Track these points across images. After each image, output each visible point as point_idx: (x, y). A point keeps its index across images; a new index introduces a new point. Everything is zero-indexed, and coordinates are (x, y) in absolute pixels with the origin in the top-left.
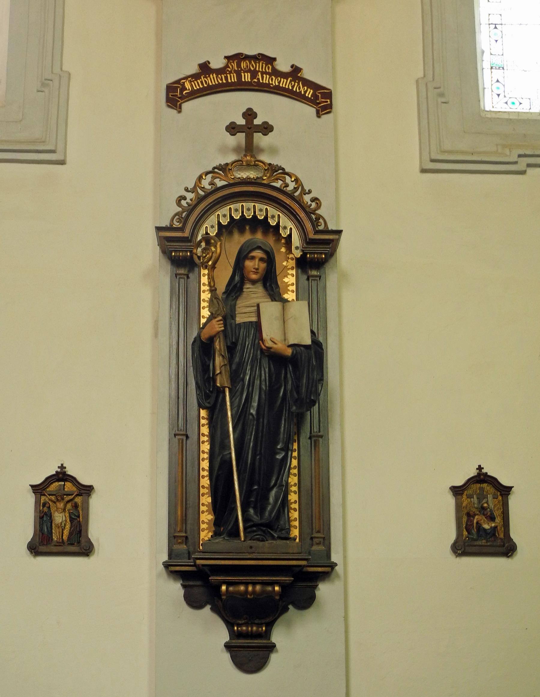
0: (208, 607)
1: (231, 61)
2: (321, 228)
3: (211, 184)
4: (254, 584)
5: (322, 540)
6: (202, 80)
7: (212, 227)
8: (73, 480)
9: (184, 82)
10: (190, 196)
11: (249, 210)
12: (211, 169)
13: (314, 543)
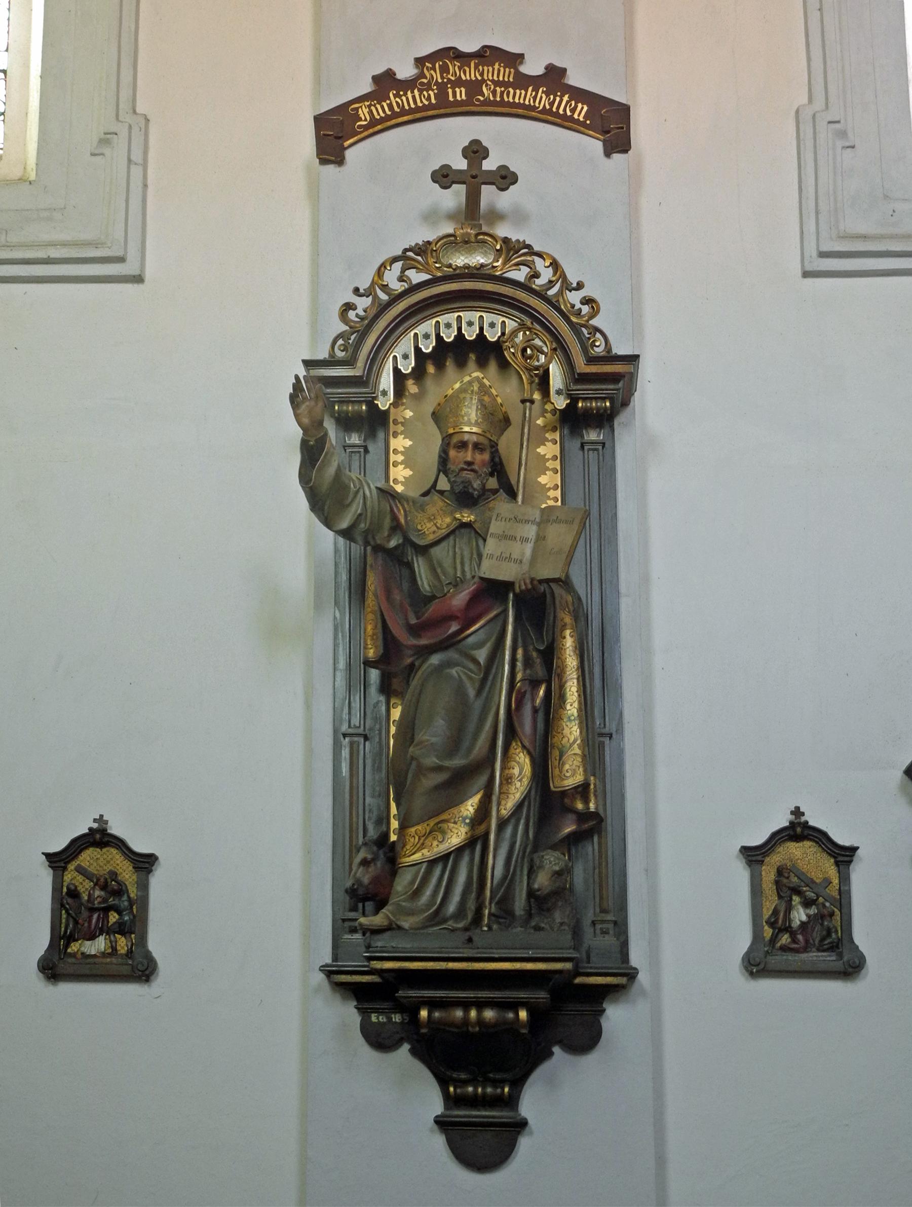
0: (406, 1047)
2: (600, 350)
3: (401, 279)
4: (481, 1005)
5: (611, 926)
6: (391, 103)
7: (406, 357)
8: (120, 844)
9: (357, 109)
10: (363, 303)
11: (448, 326)
12: (400, 253)
13: (598, 931)
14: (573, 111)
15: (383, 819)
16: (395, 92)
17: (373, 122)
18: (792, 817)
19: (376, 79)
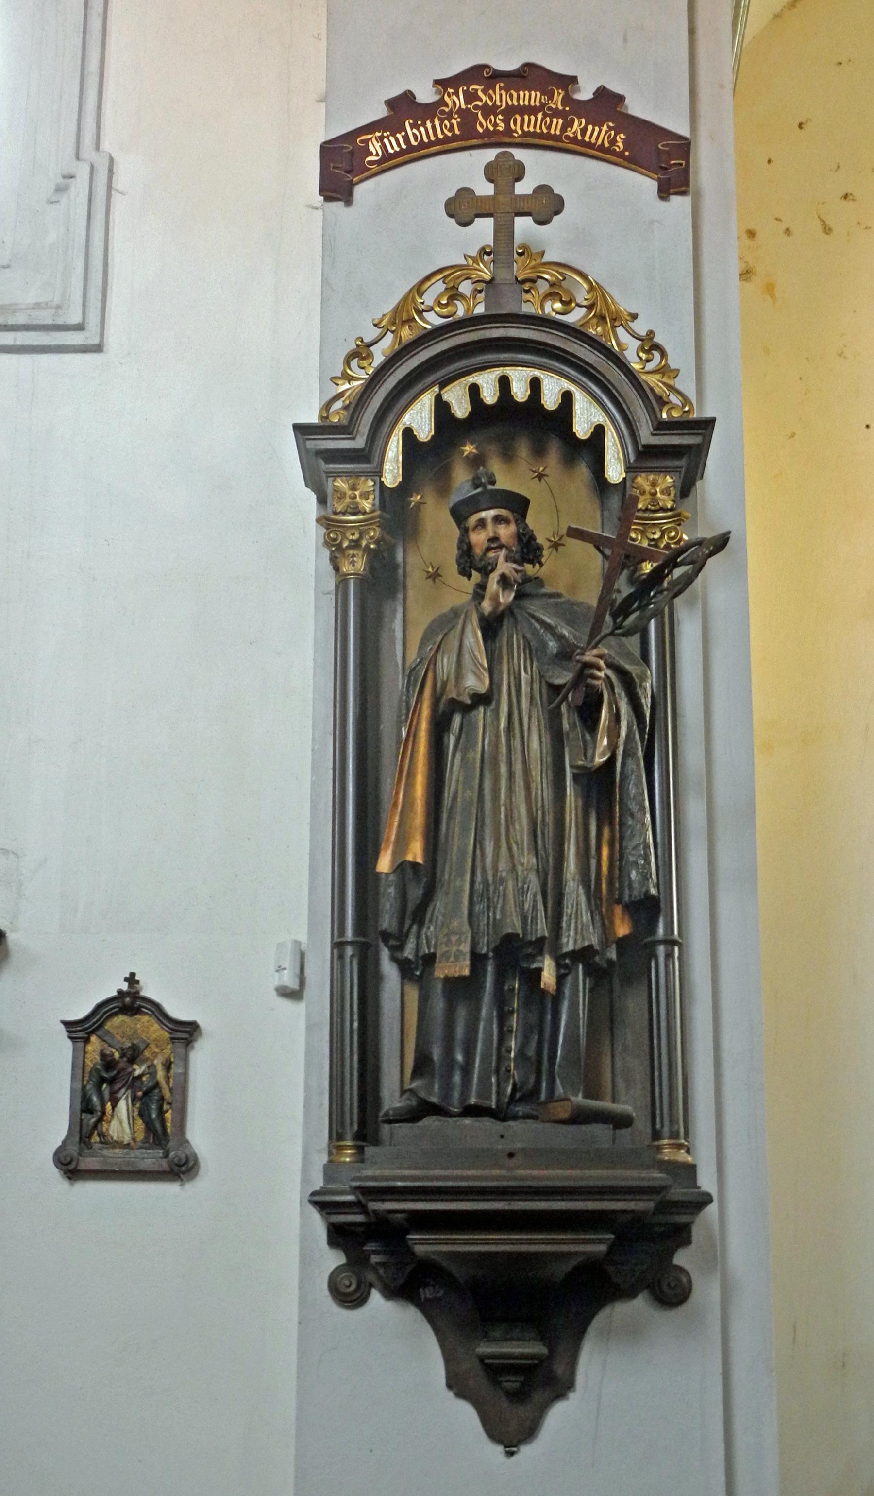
1: (451, 91)
9: (366, 142)
14: (549, 128)
15: (364, 937)
16: (411, 122)
17: (387, 157)
18: (125, 987)
19: (391, 103)
